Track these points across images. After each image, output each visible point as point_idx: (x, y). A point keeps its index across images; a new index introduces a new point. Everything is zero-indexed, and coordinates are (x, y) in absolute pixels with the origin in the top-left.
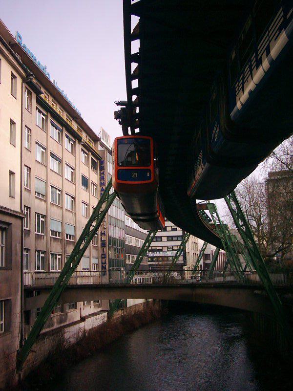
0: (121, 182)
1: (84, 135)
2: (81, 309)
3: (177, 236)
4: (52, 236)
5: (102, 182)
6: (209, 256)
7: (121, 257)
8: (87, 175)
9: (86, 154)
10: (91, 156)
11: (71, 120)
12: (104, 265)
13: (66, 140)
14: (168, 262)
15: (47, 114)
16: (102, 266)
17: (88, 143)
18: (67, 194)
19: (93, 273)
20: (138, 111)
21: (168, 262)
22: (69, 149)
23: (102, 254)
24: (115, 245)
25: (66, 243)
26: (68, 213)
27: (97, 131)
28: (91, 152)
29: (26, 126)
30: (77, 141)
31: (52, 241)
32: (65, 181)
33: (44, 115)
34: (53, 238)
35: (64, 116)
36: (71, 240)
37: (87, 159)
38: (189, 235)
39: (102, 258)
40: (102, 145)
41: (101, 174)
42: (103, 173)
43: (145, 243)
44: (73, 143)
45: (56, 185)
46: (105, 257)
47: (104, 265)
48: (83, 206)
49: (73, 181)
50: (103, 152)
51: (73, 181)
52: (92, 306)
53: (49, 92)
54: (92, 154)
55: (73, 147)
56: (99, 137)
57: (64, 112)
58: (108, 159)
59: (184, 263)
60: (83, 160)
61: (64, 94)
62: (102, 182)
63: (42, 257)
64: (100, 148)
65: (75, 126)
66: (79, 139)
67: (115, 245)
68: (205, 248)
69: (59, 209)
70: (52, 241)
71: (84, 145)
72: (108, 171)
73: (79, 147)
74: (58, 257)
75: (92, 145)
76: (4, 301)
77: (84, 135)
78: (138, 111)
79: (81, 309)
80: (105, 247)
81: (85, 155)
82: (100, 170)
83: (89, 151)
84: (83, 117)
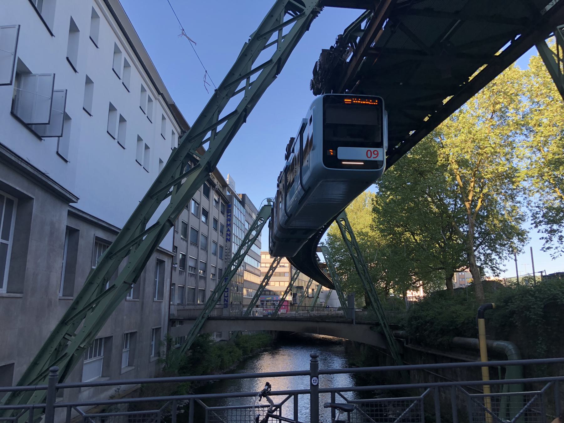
3: (285, 273)
5: (229, 223)
6: (493, 397)
8: (217, 218)
12: (226, 298)
20: (426, 119)
29: (56, 358)
30: (211, 187)
31: (189, 277)
32: (201, 222)
38: (299, 273)
40: (230, 190)
41: (228, 216)
42: (230, 216)
47: (226, 298)
48: (213, 244)
50: (231, 197)
58: (235, 203)
62: (229, 223)
64: (228, 194)
76: (131, 333)
78: (426, 119)
82: (228, 212)
84: (141, 199)
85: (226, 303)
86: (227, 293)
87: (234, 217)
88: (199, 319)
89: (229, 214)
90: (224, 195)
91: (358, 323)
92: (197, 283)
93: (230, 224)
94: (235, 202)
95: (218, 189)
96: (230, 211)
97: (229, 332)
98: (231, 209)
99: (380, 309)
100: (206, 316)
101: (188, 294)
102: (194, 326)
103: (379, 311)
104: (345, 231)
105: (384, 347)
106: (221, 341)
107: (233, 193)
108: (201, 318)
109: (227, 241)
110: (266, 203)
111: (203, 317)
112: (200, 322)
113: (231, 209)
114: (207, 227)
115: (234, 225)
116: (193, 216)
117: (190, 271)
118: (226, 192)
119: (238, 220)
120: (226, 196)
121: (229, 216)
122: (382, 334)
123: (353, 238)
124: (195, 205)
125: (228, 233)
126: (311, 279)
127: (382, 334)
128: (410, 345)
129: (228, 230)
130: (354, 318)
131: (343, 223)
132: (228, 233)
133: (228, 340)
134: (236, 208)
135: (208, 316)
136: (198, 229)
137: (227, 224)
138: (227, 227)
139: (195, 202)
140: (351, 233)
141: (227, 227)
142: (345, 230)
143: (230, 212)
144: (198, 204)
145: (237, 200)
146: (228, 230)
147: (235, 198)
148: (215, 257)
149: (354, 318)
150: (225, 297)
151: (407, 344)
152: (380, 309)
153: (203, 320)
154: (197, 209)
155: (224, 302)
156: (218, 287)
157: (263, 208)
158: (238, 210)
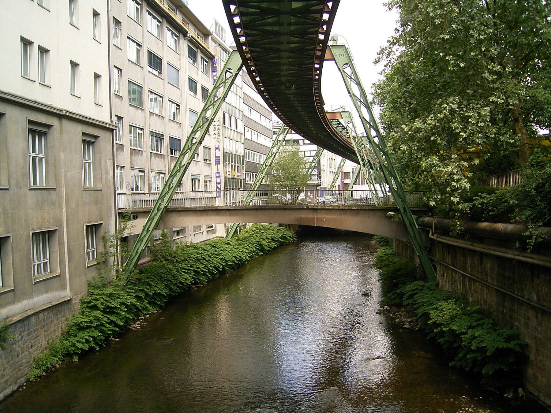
2: (190, 235)
12: (219, 186)
28: (200, 49)
30: (181, 36)
46: (219, 177)
66: (185, 33)
75: (201, 41)
88: (153, 211)
100: (162, 207)
102: (148, 221)
111: (159, 209)
112: (156, 215)
121: (215, 76)
150: (217, 183)
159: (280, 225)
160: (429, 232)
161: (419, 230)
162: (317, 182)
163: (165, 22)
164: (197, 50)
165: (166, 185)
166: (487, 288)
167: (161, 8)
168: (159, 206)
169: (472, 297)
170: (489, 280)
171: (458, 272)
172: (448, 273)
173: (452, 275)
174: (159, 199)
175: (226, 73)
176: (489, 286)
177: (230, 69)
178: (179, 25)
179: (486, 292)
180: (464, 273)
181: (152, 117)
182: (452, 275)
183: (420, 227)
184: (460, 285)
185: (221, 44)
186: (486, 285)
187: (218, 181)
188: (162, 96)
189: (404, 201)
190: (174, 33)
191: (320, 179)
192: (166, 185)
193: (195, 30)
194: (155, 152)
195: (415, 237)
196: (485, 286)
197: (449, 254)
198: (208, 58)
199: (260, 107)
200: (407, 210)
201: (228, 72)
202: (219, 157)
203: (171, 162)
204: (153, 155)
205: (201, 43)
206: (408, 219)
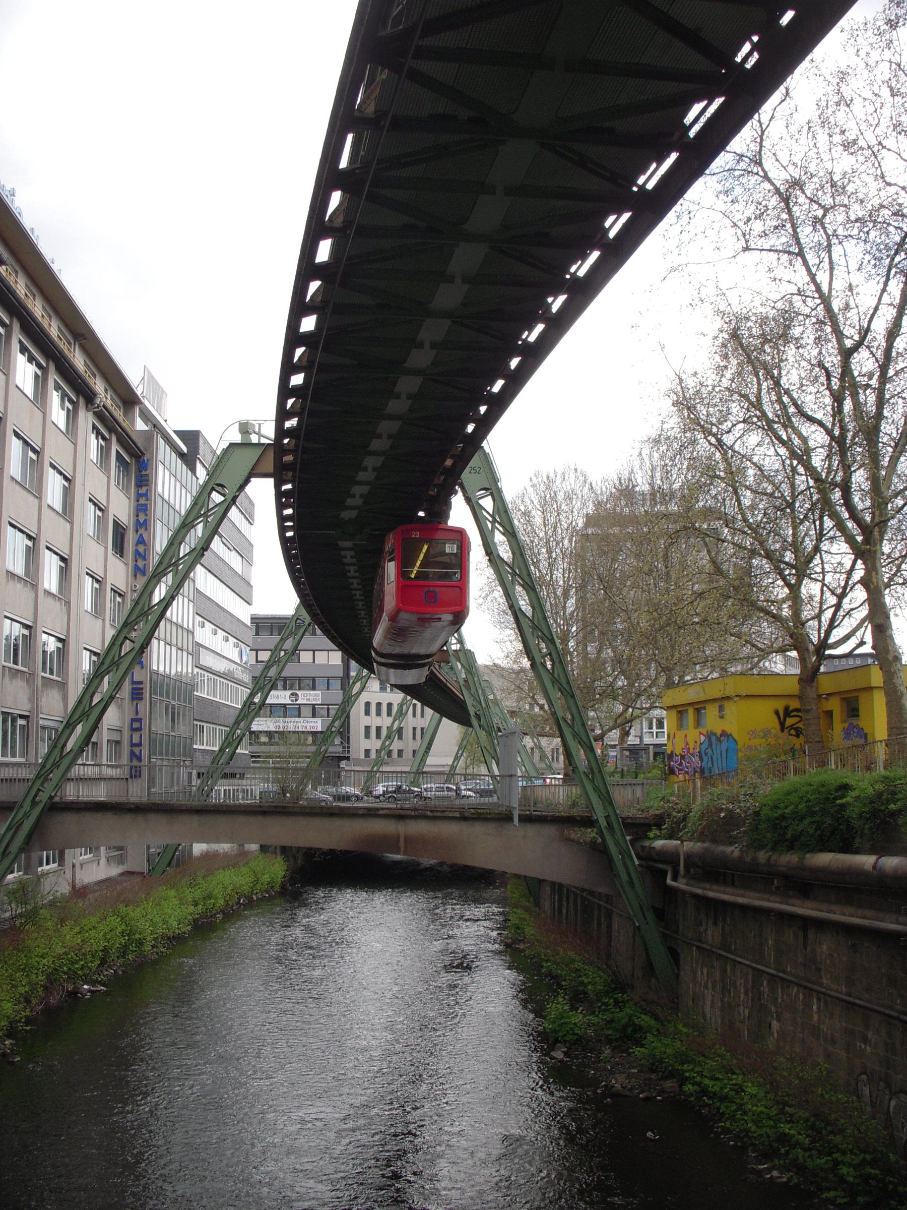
0: (402, 839)
1: (99, 386)
2: (74, 866)
4: (6, 664)
7: (183, 729)
9: (104, 438)
10: (115, 447)
11: (69, 343)
12: (136, 750)
13: (55, 398)
14: (304, 749)
15: (11, 322)
16: (132, 754)
17: (109, 407)
18: (48, 548)
19: (109, 772)
21: (304, 749)
22: (62, 423)
23: (133, 720)
24: (168, 697)
25: (43, 686)
26: (50, 600)
27: (133, 376)
28: (117, 433)
30: (82, 402)
31: (7, 677)
32: (46, 512)
33: (39, 366)
34: (10, 668)
35: (53, 329)
36: (54, 677)
37: (104, 453)
39: (133, 730)
40: (147, 417)
41: (139, 496)
42: (146, 496)
43: (252, 695)
44: (70, 407)
45: (21, 522)
46: (139, 729)
49: (68, 511)
50: (148, 437)
51: (68, 511)
52: (103, 861)
53: (18, 260)
54: (119, 441)
55: (72, 417)
56: (139, 392)
57: (20, 275)
59: (343, 752)
60: (93, 454)
61: (55, 267)
63: (22, 727)
64: (140, 425)
65: (79, 360)
66: (89, 396)
67: (185, 701)
68: (537, 603)
69: (29, 588)
70: (7, 677)
71: (99, 416)
72: (160, 489)
73: (86, 419)
74: (21, 722)
75: (119, 414)
77: (99, 386)
79: (74, 866)
80: (141, 699)
81: (101, 441)
83: (111, 430)
85: (135, 763)
86: (138, 734)
87: (159, 500)
88: (21, 806)
89: (143, 490)
90: (128, 429)
91: (526, 819)
92: (34, 698)
93: (146, 520)
94: (162, 449)
95: (104, 406)
96: (148, 481)
97: (148, 848)
98: (147, 475)
99: (597, 775)
100: (43, 797)
101: (864, 918)
102: (8, 829)
103: (592, 781)
104: (492, 531)
105: (602, 889)
106: (122, 874)
107: (156, 426)
108: (27, 805)
109: (135, 576)
110: (237, 438)
111: (34, 803)
112: (27, 815)
113: (147, 475)
114: (68, 526)
115: (159, 524)
116: (18, 487)
117: (46, 673)
118: (133, 422)
119: (171, 511)
120: (134, 437)
121: (142, 495)
122: (599, 850)
123: (518, 554)
124: (25, 455)
125: (141, 549)
126: (409, 698)
127: (599, 850)
128: (684, 881)
129: (141, 541)
130: (515, 804)
131: (487, 503)
132: (141, 549)
133: (146, 870)
134: (167, 473)
135: (51, 798)
136: (67, 551)
137: (138, 520)
138: (137, 531)
139: (26, 442)
140: (511, 534)
141: (137, 531)
142: (494, 527)
143: (147, 485)
144: (34, 451)
145: (174, 455)
146: (141, 541)
147: (161, 442)
148: (99, 623)
149: (515, 804)
150: (132, 745)
151: (675, 879)
152: (597, 775)
153: (37, 811)
154: (68, 493)
155: (131, 761)
156: (81, 709)
157: (225, 451)
158: (184, 491)
159: (263, 848)
160: (666, 872)
161: (640, 869)
162: (341, 749)
163: (52, 368)
164: (110, 436)
165: (55, 746)
166: (819, 999)
167: (43, 331)
168: (36, 796)
169: (778, 1020)
170: (825, 981)
171: (740, 963)
172: (712, 967)
173: (724, 971)
174: (38, 777)
175: (210, 494)
176: (825, 994)
177: (219, 485)
178: (76, 372)
179: (819, 1008)
180: (759, 967)
181: (11, 582)
182: (724, 971)
183: (643, 863)
184: (746, 993)
185: (157, 425)
186: (818, 992)
187: (136, 740)
188: (34, 536)
189: (608, 800)
190: (67, 395)
191: (349, 743)
192: (55, 746)
193: (106, 390)
194: (11, 665)
195: (631, 883)
196: (815, 994)
197: (715, 923)
198: (131, 455)
199: (228, 572)
200: (616, 826)
201: (214, 492)
202: (141, 683)
203: (42, 691)
204: (7, 672)
205: (117, 417)
206: (617, 844)
